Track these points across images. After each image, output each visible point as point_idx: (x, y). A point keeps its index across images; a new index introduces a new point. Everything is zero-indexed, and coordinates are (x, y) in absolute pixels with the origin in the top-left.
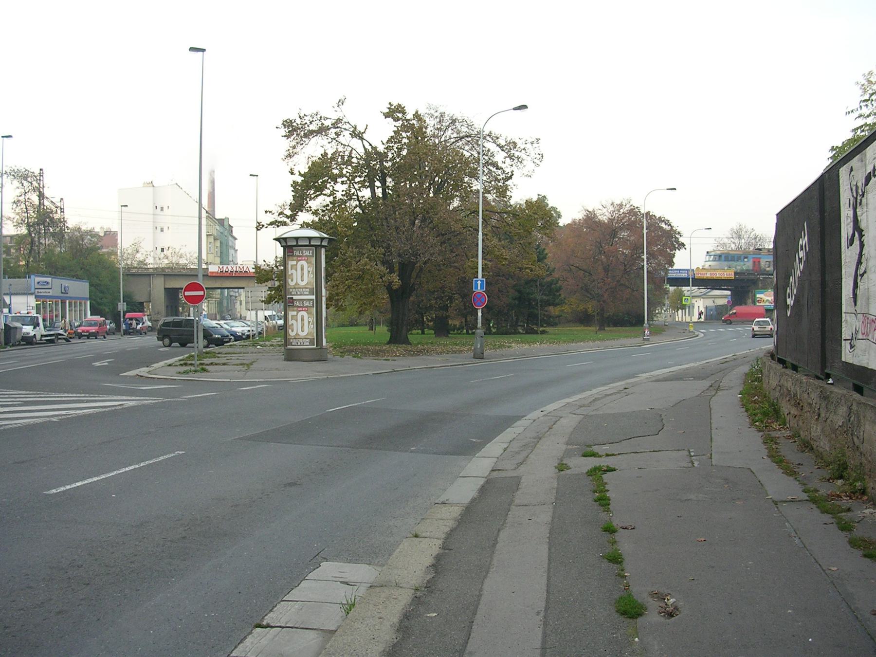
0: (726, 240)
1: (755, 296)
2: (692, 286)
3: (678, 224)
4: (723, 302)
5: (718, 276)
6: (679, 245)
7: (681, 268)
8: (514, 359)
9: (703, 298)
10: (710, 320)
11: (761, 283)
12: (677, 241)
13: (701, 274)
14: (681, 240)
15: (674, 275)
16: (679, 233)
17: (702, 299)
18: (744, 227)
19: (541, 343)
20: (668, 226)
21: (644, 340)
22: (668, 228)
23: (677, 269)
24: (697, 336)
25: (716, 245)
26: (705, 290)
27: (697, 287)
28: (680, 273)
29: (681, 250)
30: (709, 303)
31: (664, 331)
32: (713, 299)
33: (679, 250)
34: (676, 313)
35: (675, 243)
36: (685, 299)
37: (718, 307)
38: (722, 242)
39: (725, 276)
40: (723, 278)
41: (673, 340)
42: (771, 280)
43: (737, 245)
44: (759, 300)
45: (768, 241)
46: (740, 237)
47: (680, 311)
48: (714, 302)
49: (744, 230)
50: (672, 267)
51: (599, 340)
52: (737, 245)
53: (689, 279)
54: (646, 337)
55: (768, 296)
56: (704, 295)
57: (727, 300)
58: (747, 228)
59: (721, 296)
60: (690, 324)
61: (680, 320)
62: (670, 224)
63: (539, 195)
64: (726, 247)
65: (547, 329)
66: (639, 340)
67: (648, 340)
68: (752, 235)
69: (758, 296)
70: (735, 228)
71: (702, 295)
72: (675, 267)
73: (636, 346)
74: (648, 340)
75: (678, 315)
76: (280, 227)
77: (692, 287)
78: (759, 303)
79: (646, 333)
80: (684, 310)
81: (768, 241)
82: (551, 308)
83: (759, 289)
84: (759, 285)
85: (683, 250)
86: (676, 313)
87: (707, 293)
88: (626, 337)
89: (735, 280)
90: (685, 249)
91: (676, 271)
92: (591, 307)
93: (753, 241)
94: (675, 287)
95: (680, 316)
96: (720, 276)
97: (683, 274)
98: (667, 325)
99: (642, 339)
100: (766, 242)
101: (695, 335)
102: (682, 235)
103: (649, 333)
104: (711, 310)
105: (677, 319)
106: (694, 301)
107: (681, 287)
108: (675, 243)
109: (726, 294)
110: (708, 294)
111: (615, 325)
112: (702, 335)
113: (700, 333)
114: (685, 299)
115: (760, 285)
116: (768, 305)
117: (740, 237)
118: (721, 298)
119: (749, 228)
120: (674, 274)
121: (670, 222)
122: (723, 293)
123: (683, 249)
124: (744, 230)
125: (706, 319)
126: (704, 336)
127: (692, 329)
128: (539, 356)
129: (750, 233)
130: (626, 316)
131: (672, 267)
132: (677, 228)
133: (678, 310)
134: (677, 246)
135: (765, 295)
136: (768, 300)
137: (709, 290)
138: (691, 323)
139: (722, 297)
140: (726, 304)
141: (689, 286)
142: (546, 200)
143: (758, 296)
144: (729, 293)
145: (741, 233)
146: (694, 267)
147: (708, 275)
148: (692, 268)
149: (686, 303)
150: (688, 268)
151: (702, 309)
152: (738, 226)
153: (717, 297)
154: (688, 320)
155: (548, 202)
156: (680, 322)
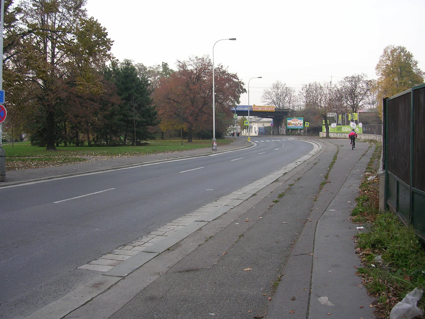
0: (270, 90)
1: (286, 121)
2: (250, 116)
3: (242, 77)
4: (269, 125)
5: (265, 109)
6: (243, 90)
7: (245, 105)
8: (50, 179)
9: (257, 123)
10: (260, 135)
11: (290, 114)
12: (241, 87)
13: (256, 108)
14: (244, 87)
15: (240, 109)
16: (243, 83)
17: (257, 124)
18: (280, 82)
19: (123, 155)
20: (237, 79)
21: (213, 150)
22: (237, 81)
23: (242, 105)
24: (253, 145)
25: (265, 93)
26: (259, 118)
27: (254, 116)
28: (244, 108)
29: (244, 93)
30: (261, 125)
31: (233, 142)
32: (263, 123)
33: (243, 93)
34: (243, 131)
35: (240, 89)
36: (246, 122)
37: (265, 128)
38: (268, 91)
39: (270, 110)
40: (268, 111)
41: (234, 149)
42: (295, 112)
43: (276, 92)
44: (289, 124)
45: (293, 91)
46: (278, 88)
47: (245, 130)
48: (263, 125)
49: (280, 84)
50: (239, 104)
51: (178, 150)
52: (276, 92)
53: (248, 111)
54: (214, 148)
55: (294, 121)
56: (258, 121)
57: (270, 124)
58: (282, 83)
59: (266, 122)
60: (248, 138)
61: (245, 135)
62: (238, 78)
63: (163, 62)
64: (270, 94)
65: (149, 142)
66: (209, 150)
67: (216, 150)
68: (284, 87)
69: (288, 121)
70: (275, 83)
71: (257, 121)
72: (241, 104)
73: (203, 156)
74: (216, 150)
75: (243, 132)
76: (316, 151)
77: (250, 116)
78: (288, 125)
79: (214, 144)
80: (247, 130)
81: (293, 91)
82: (150, 127)
83: (288, 117)
84: (288, 115)
85: (245, 94)
86: (243, 131)
87: (259, 120)
88: (202, 147)
89: (275, 112)
90: (246, 93)
91: (241, 107)
92: (185, 126)
93: (285, 91)
94: (242, 116)
95: (244, 133)
96: (267, 110)
97: (246, 109)
98: (236, 138)
99: (212, 149)
100: (292, 91)
101: (251, 145)
102: (244, 84)
103: (216, 144)
104: (262, 129)
105: (243, 135)
106: (252, 124)
107: (245, 116)
108: (240, 89)
109: (270, 120)
110: (260, 121)
111: (203, 138)
112: (256, 145)
113: (254, 143)
114: (246, 122)
115: (289, 115)
116: (294, 127)
117: (278, 88)
118: (267, 122)
119: (283, 83)
120: (241, 109)
121: (238, 77)
122: (268, 120)
123: (245, 93)
124: (280, 84)
125: (259, 134)
126: (257, 145)
127: (249, 141)
128: (89, 172)
129: (284, 86)
130: (210, 132)
131: (239, 104)
132: (241, 80)
133: (244, 129)
134: (241, 90)
135: (292, 121)
136: (294, 124)
137: (261, 118)
138: (249, 137)
139: (268, 122)
140: (270, 126)
141: (248, 116)
142: (168, 66)
143: (288, 121)
144: (271, 120)
145: (278, 86)
146: (251, 104)
147: (260, 109)
148: (250, 105)
149: (246, 125)
150: (248, 105)
151: (257, 129)
152: (277, 82)
153: (266, 122)
154: (247, 134)
155: (169, 67)
156: (245, 136)
